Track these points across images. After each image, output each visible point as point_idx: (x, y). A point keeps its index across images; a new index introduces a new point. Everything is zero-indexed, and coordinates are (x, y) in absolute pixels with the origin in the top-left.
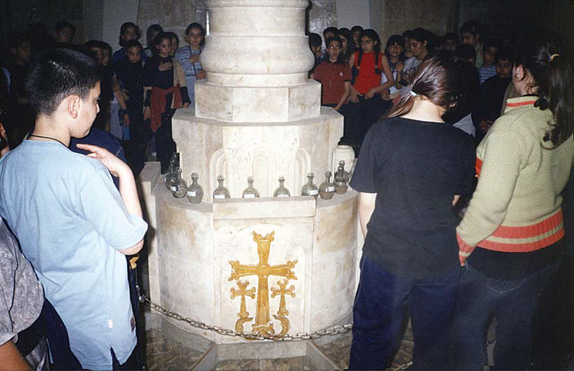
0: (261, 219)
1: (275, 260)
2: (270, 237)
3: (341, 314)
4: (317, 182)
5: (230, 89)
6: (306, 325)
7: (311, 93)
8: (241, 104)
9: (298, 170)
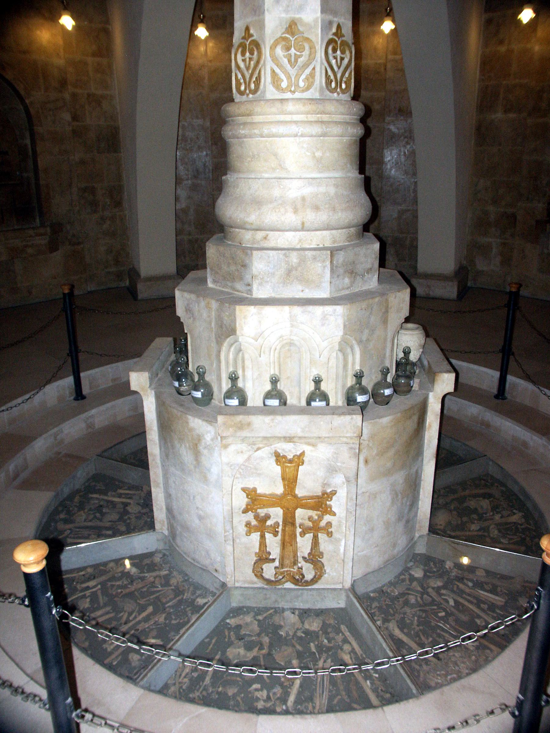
0: (285, 438)
1: (308, 484)
2: (299, 460)
3: (396, 551)
4: (368, 382)
5: (249, 252)
6: (346, 572)
7: (366, 256)
8: (264, 272)
9: (341, 366)
